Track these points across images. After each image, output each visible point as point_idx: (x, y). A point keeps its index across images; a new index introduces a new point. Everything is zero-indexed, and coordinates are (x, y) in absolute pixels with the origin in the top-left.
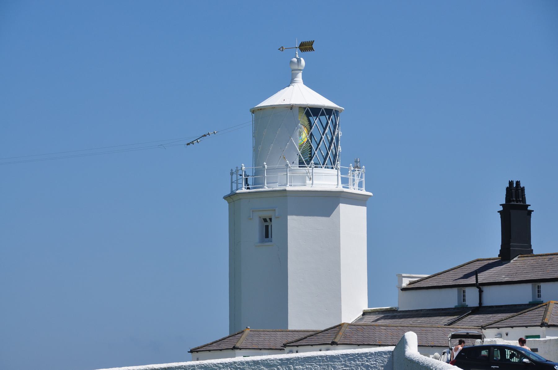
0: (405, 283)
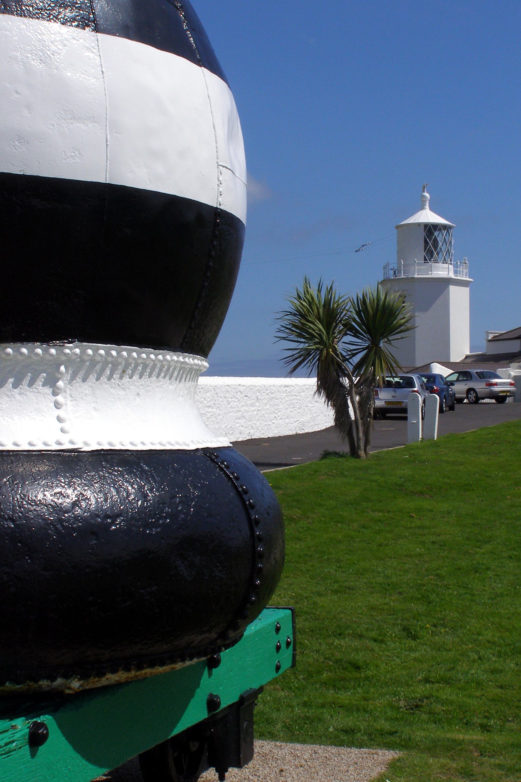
0: (490, 337)
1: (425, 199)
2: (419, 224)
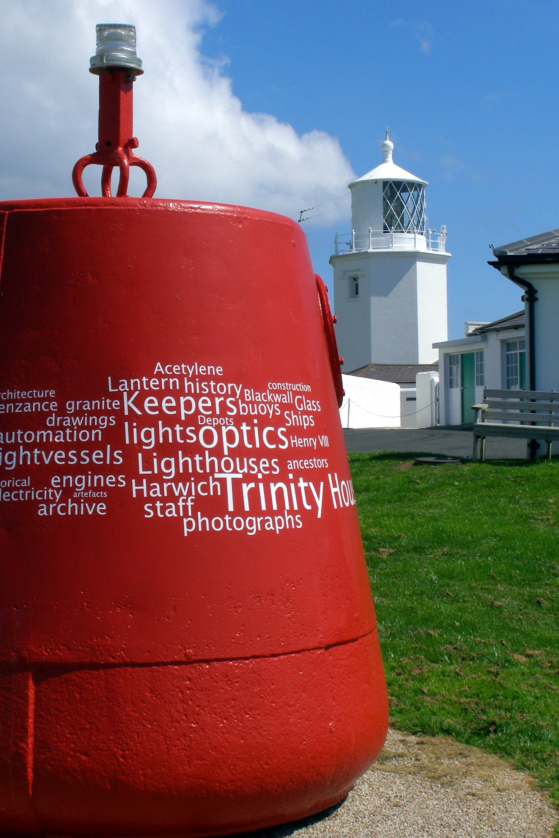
0: (471, 330)
1: (388, 149)
2: (376, 181)
